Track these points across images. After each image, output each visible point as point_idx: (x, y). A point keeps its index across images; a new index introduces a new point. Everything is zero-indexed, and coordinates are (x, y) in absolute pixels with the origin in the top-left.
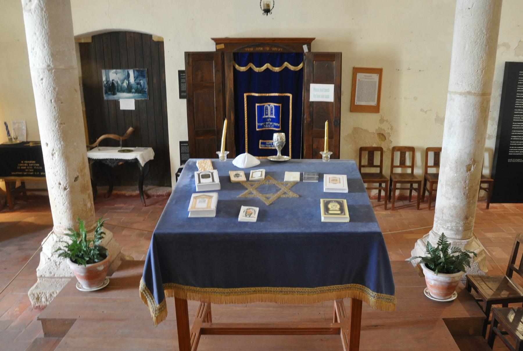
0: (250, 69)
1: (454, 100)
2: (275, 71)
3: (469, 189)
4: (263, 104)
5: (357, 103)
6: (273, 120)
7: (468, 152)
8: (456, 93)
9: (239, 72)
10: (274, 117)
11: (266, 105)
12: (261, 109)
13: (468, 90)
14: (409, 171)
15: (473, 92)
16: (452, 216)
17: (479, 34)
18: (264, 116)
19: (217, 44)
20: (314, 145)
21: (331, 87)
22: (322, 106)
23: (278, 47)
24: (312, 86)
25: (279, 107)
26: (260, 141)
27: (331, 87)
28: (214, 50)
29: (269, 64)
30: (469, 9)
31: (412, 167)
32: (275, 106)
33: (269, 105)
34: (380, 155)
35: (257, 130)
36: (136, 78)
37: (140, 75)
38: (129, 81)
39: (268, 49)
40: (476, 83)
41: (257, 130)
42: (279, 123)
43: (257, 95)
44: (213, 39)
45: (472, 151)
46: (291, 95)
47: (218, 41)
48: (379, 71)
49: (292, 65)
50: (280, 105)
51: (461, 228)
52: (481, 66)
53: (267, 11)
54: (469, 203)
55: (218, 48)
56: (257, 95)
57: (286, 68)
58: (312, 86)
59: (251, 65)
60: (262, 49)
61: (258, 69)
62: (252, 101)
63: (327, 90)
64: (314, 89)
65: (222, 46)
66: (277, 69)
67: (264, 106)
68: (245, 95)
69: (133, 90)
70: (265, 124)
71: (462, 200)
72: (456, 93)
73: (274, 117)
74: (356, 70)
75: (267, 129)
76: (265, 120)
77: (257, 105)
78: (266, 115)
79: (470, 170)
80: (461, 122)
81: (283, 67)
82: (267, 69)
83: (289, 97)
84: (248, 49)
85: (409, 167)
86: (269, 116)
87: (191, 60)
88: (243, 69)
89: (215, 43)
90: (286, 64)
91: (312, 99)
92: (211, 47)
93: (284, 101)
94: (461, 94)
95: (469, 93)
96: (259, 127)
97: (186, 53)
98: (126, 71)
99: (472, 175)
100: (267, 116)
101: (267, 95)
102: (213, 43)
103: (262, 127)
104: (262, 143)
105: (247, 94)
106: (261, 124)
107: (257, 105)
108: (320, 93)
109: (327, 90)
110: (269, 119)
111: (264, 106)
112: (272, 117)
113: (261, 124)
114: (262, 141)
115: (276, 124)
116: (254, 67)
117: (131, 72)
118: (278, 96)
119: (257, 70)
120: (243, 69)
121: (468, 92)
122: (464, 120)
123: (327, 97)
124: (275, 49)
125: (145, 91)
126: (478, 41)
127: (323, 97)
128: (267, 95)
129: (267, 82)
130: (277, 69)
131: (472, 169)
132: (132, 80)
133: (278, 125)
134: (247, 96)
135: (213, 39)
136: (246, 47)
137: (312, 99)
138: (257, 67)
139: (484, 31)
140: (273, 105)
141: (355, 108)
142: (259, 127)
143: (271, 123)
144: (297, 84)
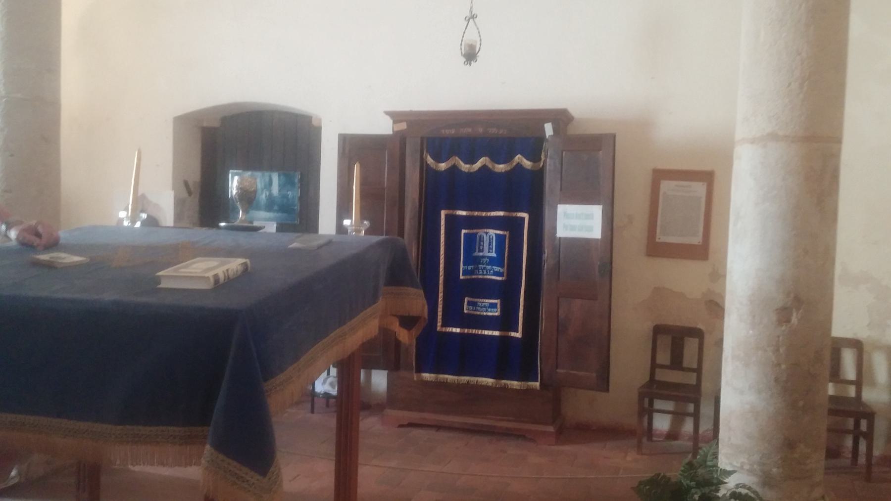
0: (454, 169)
4: (475, 231)
5: (661, 238)
10: (494, 255)
11: (481, 232)
12: (470, 239)
14: (852, 392)
18: (477, 254)
19: (394, 122)
20: (561, 311)
21: (596, 212)
22: (581, 245)
24: (562, 209)
25: (505, 236)
26: (466, 299)
27: (596, 212)
29: (487, 158)
31: (858, 384)
33: (487, 233)
34: (697, 346)
35: (462, 277)
36: (281, 187)
37: (287, 183)
38: (270, 191)
41: (462, 277)
42: (503, 267)
43: (464, 213)
44: (387, 113)
46: (525, 216)
47: (396, 117)
48: (707, 177)
50: (507, 233)
51: (775, 470)
53: (471, 56)
55: (395, 129)
56: (464, 213)
57: (519, 166)
58: (562, 209)
61: (468, 166)
62: (454, 224)
63: (589, 217)
64: (566, 215)
65: (403, 126)
66: (501, 168)
68: (443, 213)
69: (276, 208)
70: (478, 269)
73: (494, 255)
74: (659, 175)
75: (481, 277)
77: (464, 231)
78: (480, 251)
79: (788, 321)
81: (514, 164)
82: (484, 167)
83: (523, 219)
84: (447, 132)
85: (851, 383)
86: (486, 253)
88: (443, 166)
89: (391, 121)
90: (518, 158)
91: (561, 233)
93: (514, 226)
98: (267, 174)
100: (481, 254)
101: (484, 214)
103: (472, 272)
104: (469, 303)
106: (470, 268)
107: (464, 231)
108: (576, 222)
110: (485, 260)
112: (490, 255)
113: (470, 268)
114: (470, 299)
115: (497, 269)
117: (275, 178)
119: (465, 167)
123: (590, 229)
125: (294, 210)
128: (484, 214)
129: (482, 191)
130: (501, 168)
131: (794, 320)
132: (275, 190)
133: (502, 270)
134: (446, 216)
135: (387, 113)
137: (561, 233)
138: (466, 163)
140: (492, 232)
141: (656, 249)
142: (466, 272)
143: (489, 267)
144: (526, 194)
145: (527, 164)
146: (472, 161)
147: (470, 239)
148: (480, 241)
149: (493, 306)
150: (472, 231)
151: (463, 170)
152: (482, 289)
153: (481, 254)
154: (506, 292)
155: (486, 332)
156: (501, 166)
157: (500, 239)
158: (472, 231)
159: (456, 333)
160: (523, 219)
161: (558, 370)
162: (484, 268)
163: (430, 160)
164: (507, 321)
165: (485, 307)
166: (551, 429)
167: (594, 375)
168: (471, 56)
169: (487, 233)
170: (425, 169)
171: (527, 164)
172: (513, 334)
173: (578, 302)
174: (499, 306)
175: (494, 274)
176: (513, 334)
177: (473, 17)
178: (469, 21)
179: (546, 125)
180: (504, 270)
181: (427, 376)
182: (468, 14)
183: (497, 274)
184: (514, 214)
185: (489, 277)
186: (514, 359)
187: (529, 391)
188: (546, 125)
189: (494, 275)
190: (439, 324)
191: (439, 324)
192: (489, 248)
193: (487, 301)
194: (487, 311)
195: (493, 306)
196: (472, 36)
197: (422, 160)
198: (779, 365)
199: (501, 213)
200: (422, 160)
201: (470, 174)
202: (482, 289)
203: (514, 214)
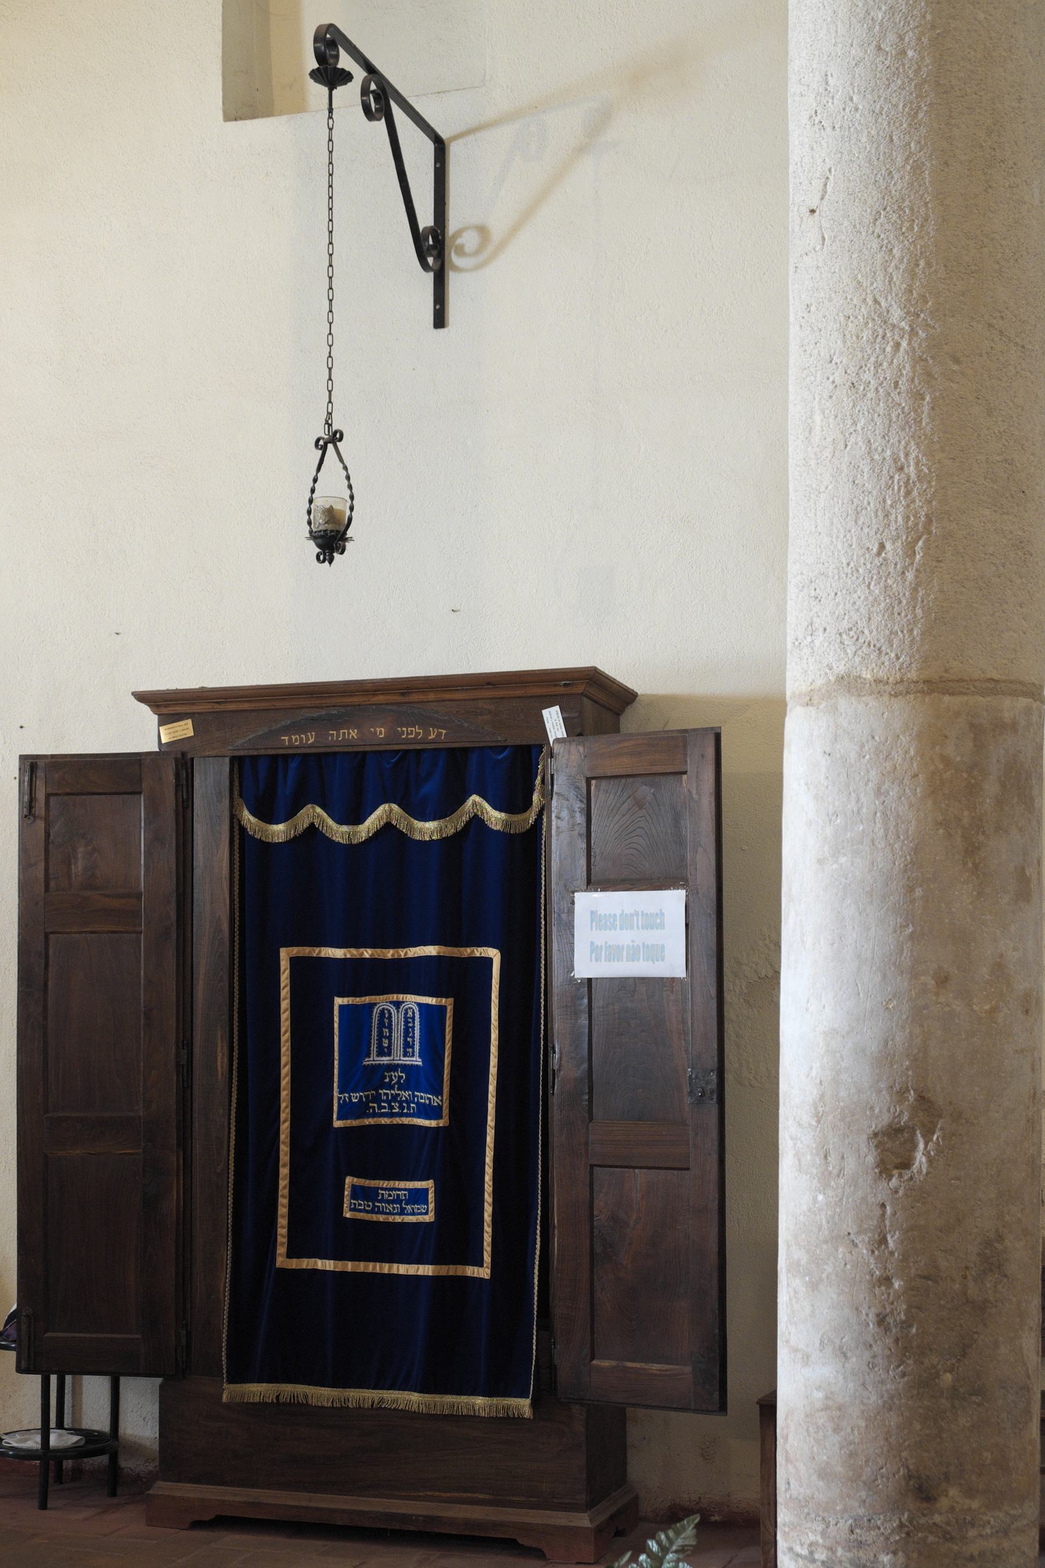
2: (417, 837)
3: (910, 1289)
4: (367, 999)
6: (413, 1078)
7: (874, 1047)
9: (266, 848)
10: (417, 1061)
11: (382, 1002)
12: (356, 1017)
13: (841, 668)
15: (867, 675)
16: (824, 1473)
17: (866, 334)
18: (374, 1059)
20: (599, 1203)
23: (426, 721)
25: (442, 1009)
26: (349, 1180)
28: (151, 746)
30: (813, 211)
32: (419, 1005)
33: (398, 1004)
35: (337, 1124)
39: (381, 732)
40: (877, 618)
41: (337, 1124)
42: (438, 1092)
43: (338, 953)
44: (142, 697)
45: (900, 1038)
46: (494, 954)
47: (166, 705)
49: (495, 808)
50: (448, 1003)
52: (898, 516)
53: (331, 540)
54: (923, 1385)
56: (338, 953)
57: (477, 822)
59: (313, 814)
60: (354, 734)
61: (345, 828)
65: (185, 729)
66: (428, 829)
67: (372, 1005)
70: (377, 1099)
71: (871, 1366)
73: (417, 1061)
75: (384, 1121)
76: (375, 1078)
78: (381, 1053)
79: (906, 1164)
80: (821, 862)
82: (388, 828)
83: (489, 961)
87: (41, 795)
88: (279, 831)
92: (143, 734)
93: (462, 981)
95: (848, 683)
96: (347, 1111)
97: (32, 767)
99: (918, 1195)
100: (385, 1060)
102: (148, 716)
105: (295, 951)
109: (655, 921)
111: (372, 1005)
112: (407, 1061)
115: (424, 1097)
116: (330, 822)
118: (438, 959)
119: (339, 832)
120: (279, 831)
121: (841, 679)
122: (836, 853)
123: (656, 952)
124: (412, 734)
126: (867, 376)
127: (634, 954)
129: (384, 890)
130: (428, 829)
131: (920, 1159)
133: (435, 1101)
134: (294, 961)
135: (142, 697)
136: (287, 730)
138: (340, 822)
139: (896, 314)
140: (412, 1000)
143: (405, 1094)
144: (506, 895)
145: (495, 817)
146: (356, 818)
147: (356, 1017)
148: (381, 1025)
149: (419, 1196)
150: (358, 1001)
151: (337, 839)
152: (388, 1152)
153: (385, 1060)
154: (450, 1156)
155: (403, 1269)
156: (431, 825)
157: (432, 1016)
158: (358, 1001)
159: (324, 1272)
160: (489, 961)
161: (594, 1362)
162: (395, 1097)
163: (248, 818)
164: (453, 1237)
165: (398, 1200)
166: (583, 1521)
167: (688, 1369)
168: (331, 540)
169: (398, 1004)
170: (243, 842)
171: (495, 817)
172: (471, 1271)
173: (641, 1177)
174: (431, 1196)
175: (423, 1115)
176: (471, 1271)
177: (336, 437)
178: (324, 449)
179: (545, 713)
180: (443, 1100)
181: (258, 1391)
182: (321, 432)
183: (427, 1111)
184: (467, 952)
185: (406, 1121)
186: (481, 1335)
187: (511, 1421)
188: (545, 713)
189: (418, 1115)
190: (281, 1250)
191: (281, 1250)
192: (407, 1045)
193: (402, 1184)
194: (402, 1212)
195: (419, 1196)
196: (331, 490)
197: (234, 820)
198: (886, 1281)
199: (431, 950)
200: (234, 820)
201: (352, 850)
202: (388, 1152)
203: (467, 952)
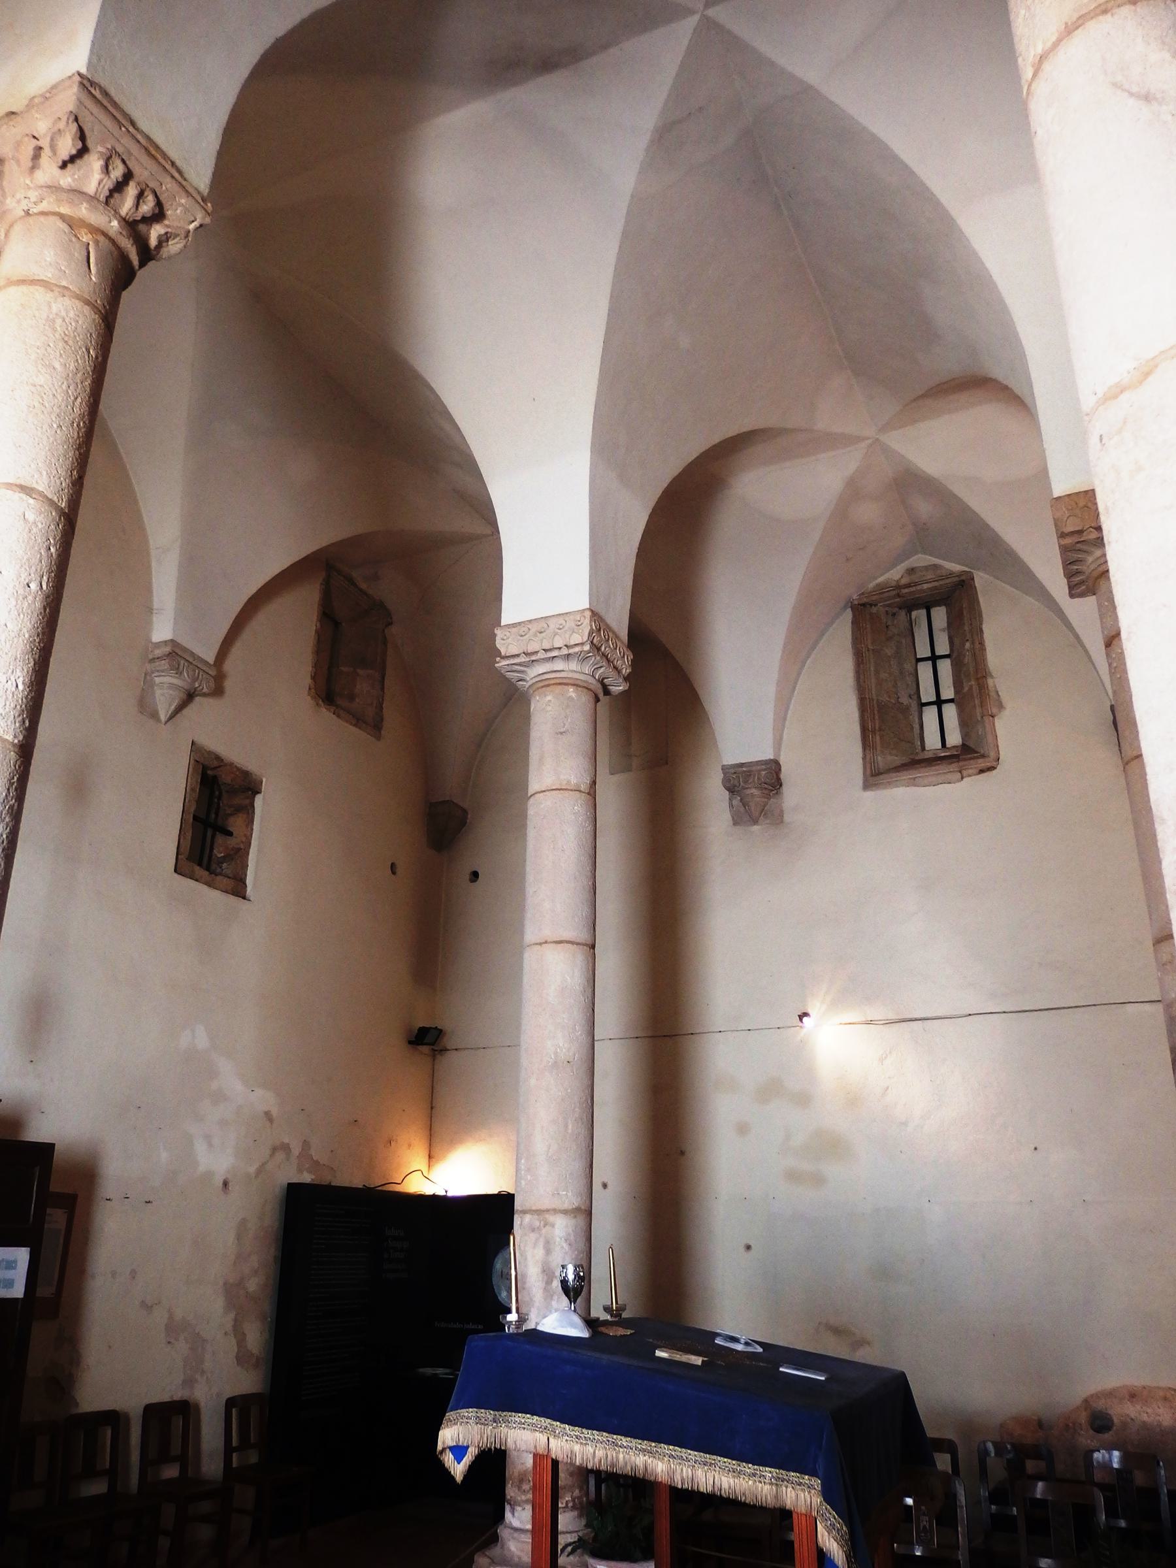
1: (553, 1226)
8: (555, 1211)
72: (555, 1211)
94: (565, 1212)
123: (9, 1284)
